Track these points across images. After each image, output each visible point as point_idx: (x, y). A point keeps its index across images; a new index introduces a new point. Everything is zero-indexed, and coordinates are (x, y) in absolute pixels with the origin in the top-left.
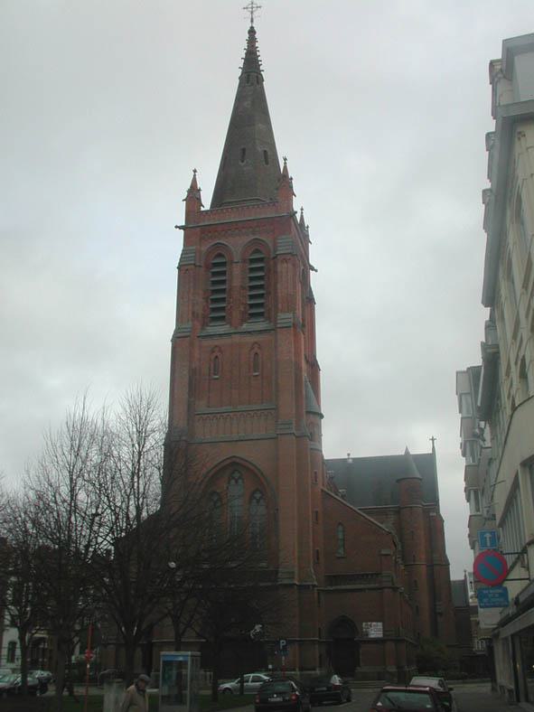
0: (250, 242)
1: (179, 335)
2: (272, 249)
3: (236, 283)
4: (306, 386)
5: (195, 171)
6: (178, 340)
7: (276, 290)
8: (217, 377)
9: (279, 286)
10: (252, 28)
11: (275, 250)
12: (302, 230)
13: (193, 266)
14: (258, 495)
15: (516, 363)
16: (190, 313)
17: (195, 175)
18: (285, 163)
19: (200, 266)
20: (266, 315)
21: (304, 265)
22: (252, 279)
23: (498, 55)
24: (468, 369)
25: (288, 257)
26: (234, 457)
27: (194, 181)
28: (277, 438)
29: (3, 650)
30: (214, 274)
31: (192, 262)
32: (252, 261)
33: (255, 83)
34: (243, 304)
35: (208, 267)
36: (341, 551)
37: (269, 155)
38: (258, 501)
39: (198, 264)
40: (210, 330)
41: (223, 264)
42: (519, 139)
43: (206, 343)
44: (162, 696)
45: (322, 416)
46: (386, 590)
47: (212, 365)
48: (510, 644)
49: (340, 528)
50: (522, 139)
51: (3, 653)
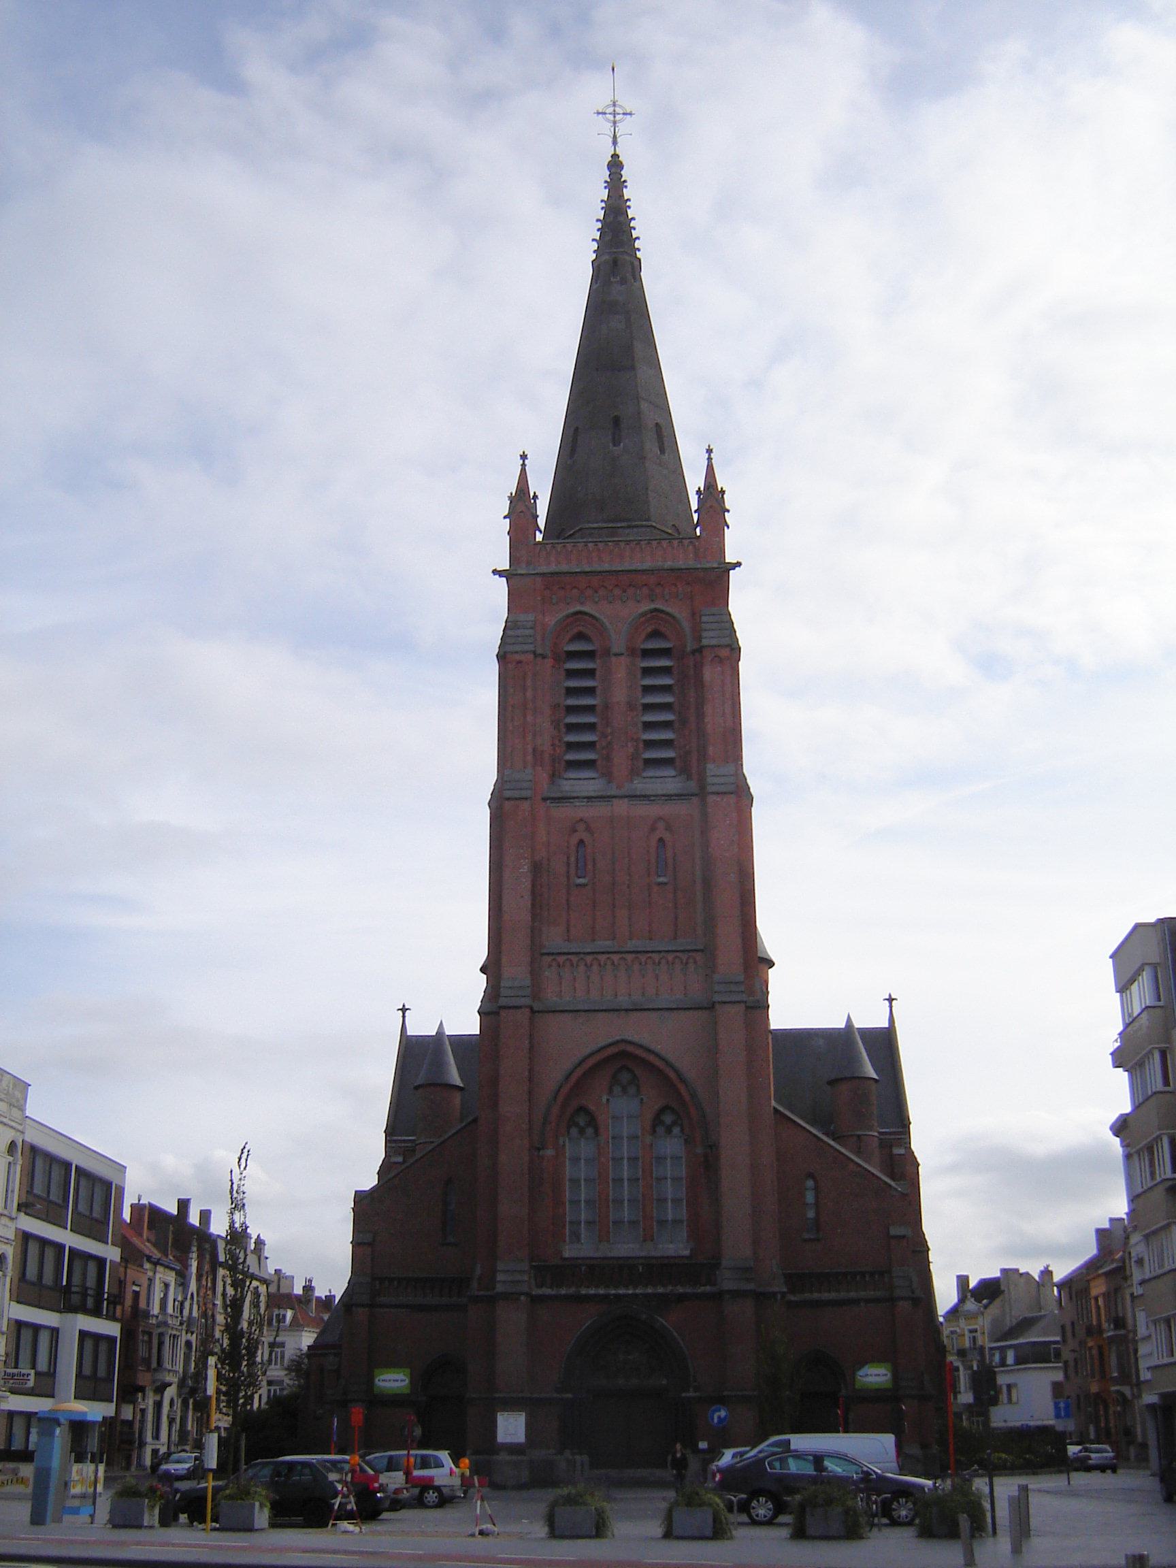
0: (644, 614)
1: (508, 794)
3: (620, 695)
6: (503, 807)
7: (700, 715)
9: (708, 709)
11: (700, 638)
14: (668, 1119)
16: (530, 750)
19: (544, 657)
26: (623, 1041)
30: (571, 674)
31: (531, 647)
32: (646, 653)
38: (669, 1130)
39: (539, 651)
40: (639, 786)
41: (590, 655)
45: (771, 964)
46: (901, 1303)
47: (573, 859)
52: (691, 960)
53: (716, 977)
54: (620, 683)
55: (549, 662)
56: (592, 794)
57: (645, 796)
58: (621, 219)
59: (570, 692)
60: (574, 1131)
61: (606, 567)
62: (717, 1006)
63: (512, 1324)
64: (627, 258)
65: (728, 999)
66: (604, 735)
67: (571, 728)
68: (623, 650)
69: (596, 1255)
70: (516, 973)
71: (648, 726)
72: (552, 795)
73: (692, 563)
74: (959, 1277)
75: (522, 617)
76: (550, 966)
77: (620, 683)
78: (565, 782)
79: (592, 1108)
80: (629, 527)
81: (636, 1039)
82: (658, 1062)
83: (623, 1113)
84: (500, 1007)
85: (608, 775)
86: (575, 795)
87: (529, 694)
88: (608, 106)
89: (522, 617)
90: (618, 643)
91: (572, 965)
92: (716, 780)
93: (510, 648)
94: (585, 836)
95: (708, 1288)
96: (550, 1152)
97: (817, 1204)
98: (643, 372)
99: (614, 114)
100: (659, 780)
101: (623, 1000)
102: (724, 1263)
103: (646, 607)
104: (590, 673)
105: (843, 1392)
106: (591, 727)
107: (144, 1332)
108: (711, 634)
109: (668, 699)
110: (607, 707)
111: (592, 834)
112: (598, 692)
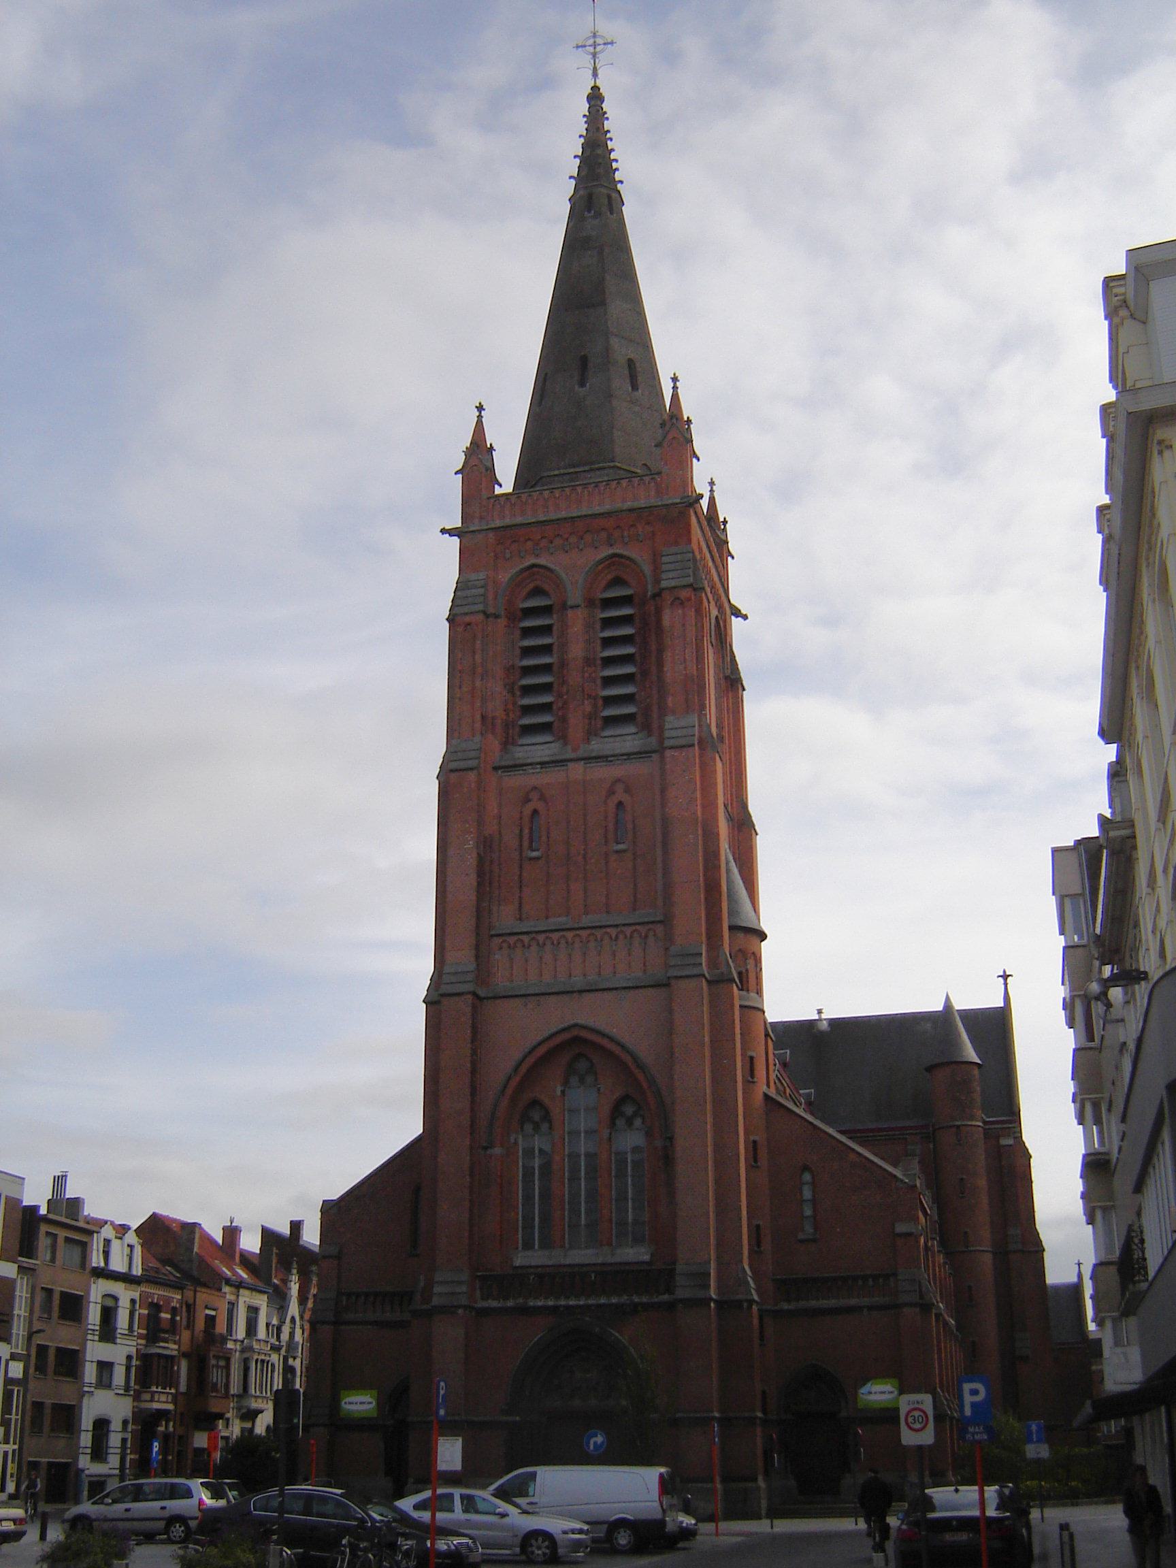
0: (601, 562)
1: (453, 765)
2: (649, 579)
3: (576, 651)
4: (728, 871)
5: (480, 408)
7: (660, 664)
8: (535, 854)
9: (668, 655)
10: (595, 88)
11: (657, 581)
12: (714, 524)
13: (481, 617)
14: (629, 1110)
15: (1165, 870)
16: (478, 717)
17: (480, 417)
18: (675, 388)
20: (639, 718)
21: (720, 608)
22: (608, 642)
23: (1119, 267)
24: (1079, 843)
25: (684, 594)
26: (575, 1025)
29: (83, 1434)
30: (527, 632)
31: (481, 607)
32: (608, 603)
33: (605, 209)
34: (589, 696)
35: (514, 616)
36: (809, 1229)
37: (641, 369)
38: (630, 1122)
39: (491, 610)
40: (597, 746)
41: (546, 610)
42: (1160, 453)
43: (516, 781)
45: (763, 936)
46: (906, 1310)
47: (526, 831)
48: (1164, 1424)
49: (807, 1177)
50: (1167, 454)
51: (82, 1444)
52: (651, 933)
53: (673, 949)
54: (577, 636)
55: (502, 622)
56: (547, 759)
57: (599, 757)
58: (599, 152)
59: (527, 652)
60: (528, 1127)
61: (563, 514)
62: (673, 982)
63: (449, 1337)
64: (604, 191)
65: (688, 973)
67: (528, 690)
68: (579, 601)
69: (550, 1263)
70: (463, 958)
71: (609, 681)
72: (503, 763)
73: (653, 501)
75: (473, 576)
76: (501, 948)
77: (577, 636)
78: (519, 749)
79: (547, 1101)
80: (591, 470)
81: (590, 1022)
82: (616, 1049)
83: (581, 1107)
84: (442, 995)
85: (563, 738)
86: (529, 761)
87: (478, 657)
88: (588, 38)
89: (473, 576)
90: (575, 595)
92: (674, 733)
93: (457, 610)
94: (540, 806)
95: (666, 1297)
96: (497, 1151)
97: (814, 1201)
98: (616, 308)
100: (618, 739)
101: (578, 981)
102: (680, 1268)
103: (606, 552)
104: (547, 630)
105: (844, 1414)
106: (547, 688)
107: (217, 1358)
108: (671, 575)
109: (630, 650)
110: (563, 664)
112: (555, 648)
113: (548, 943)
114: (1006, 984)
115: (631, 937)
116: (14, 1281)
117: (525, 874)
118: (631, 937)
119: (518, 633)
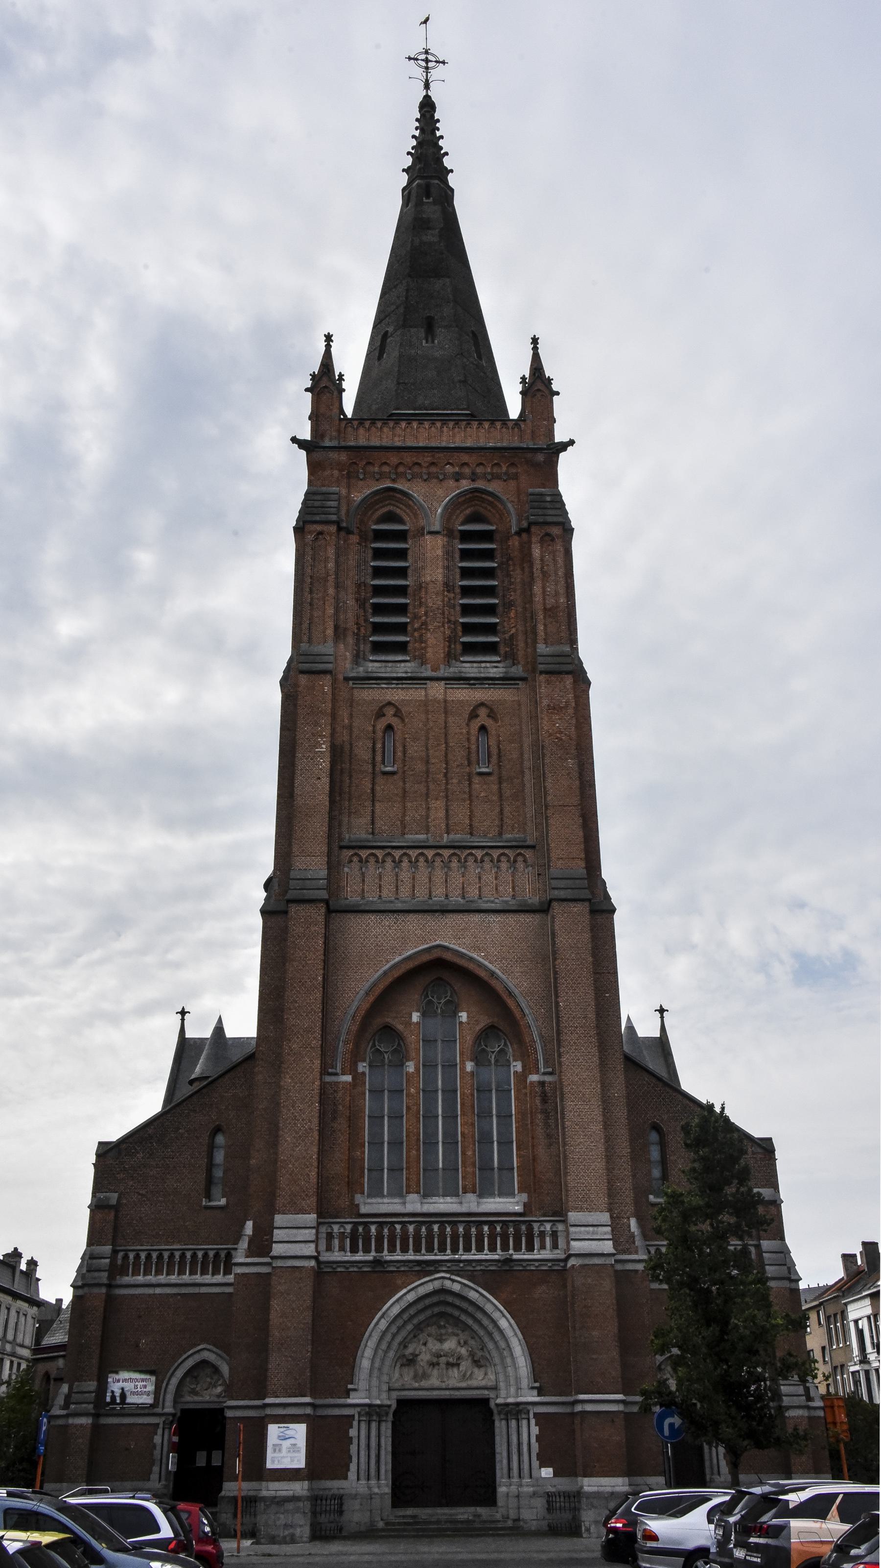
10: (427, 98)
13: (333, 528)
20: (503, 649)
27: (536, 358)
28: (286, 912)
32: (466, 536)
44: (242, 1497)
52: (520, 859)
59: (378, 572)
66: (416, 617)
67: (379, 609)
70: (313, 865)
74: (864, 1244)
76: (351, 861)
77: (432, 561)
79: (400, 1027)
84: (289, 901)
88: (421, 53)
91: (377, 862)
99: (427, 61)
103: (465, 485)
111: (403, 720)
113: (405, 859)
114: (183, 1020)
115: (499, 861)
116: (235, 1274)
117: (378, 788)
118: (499, 861)
119: (370, 553)
